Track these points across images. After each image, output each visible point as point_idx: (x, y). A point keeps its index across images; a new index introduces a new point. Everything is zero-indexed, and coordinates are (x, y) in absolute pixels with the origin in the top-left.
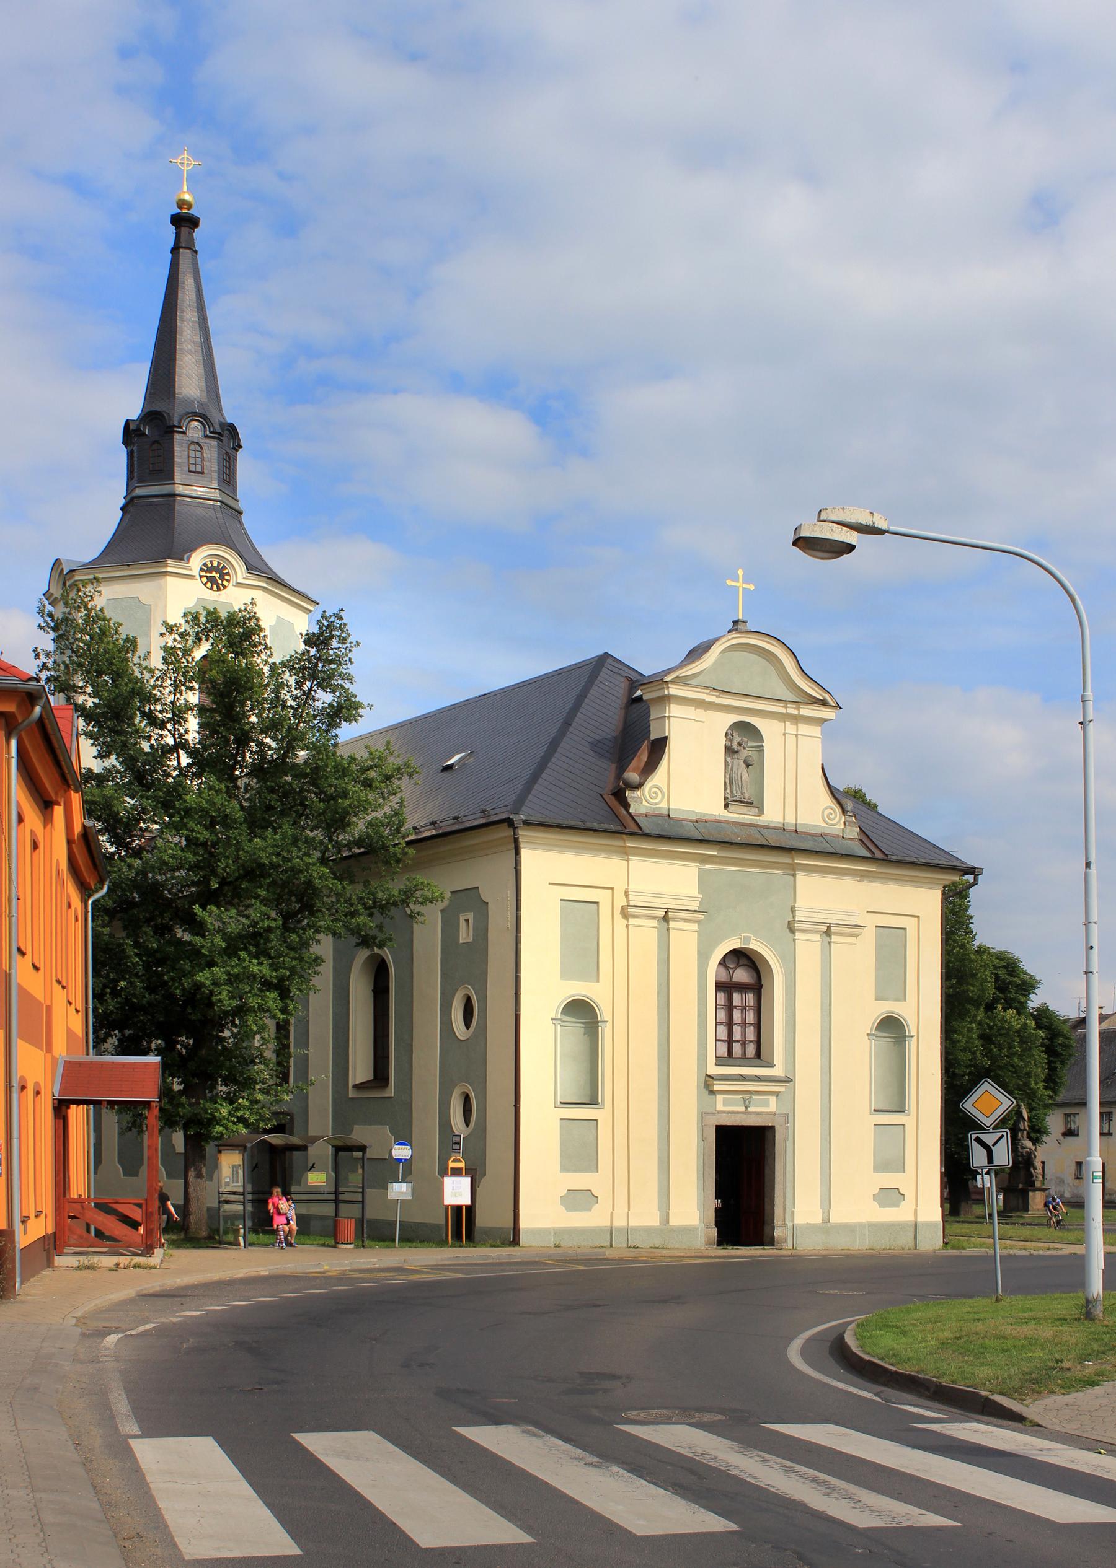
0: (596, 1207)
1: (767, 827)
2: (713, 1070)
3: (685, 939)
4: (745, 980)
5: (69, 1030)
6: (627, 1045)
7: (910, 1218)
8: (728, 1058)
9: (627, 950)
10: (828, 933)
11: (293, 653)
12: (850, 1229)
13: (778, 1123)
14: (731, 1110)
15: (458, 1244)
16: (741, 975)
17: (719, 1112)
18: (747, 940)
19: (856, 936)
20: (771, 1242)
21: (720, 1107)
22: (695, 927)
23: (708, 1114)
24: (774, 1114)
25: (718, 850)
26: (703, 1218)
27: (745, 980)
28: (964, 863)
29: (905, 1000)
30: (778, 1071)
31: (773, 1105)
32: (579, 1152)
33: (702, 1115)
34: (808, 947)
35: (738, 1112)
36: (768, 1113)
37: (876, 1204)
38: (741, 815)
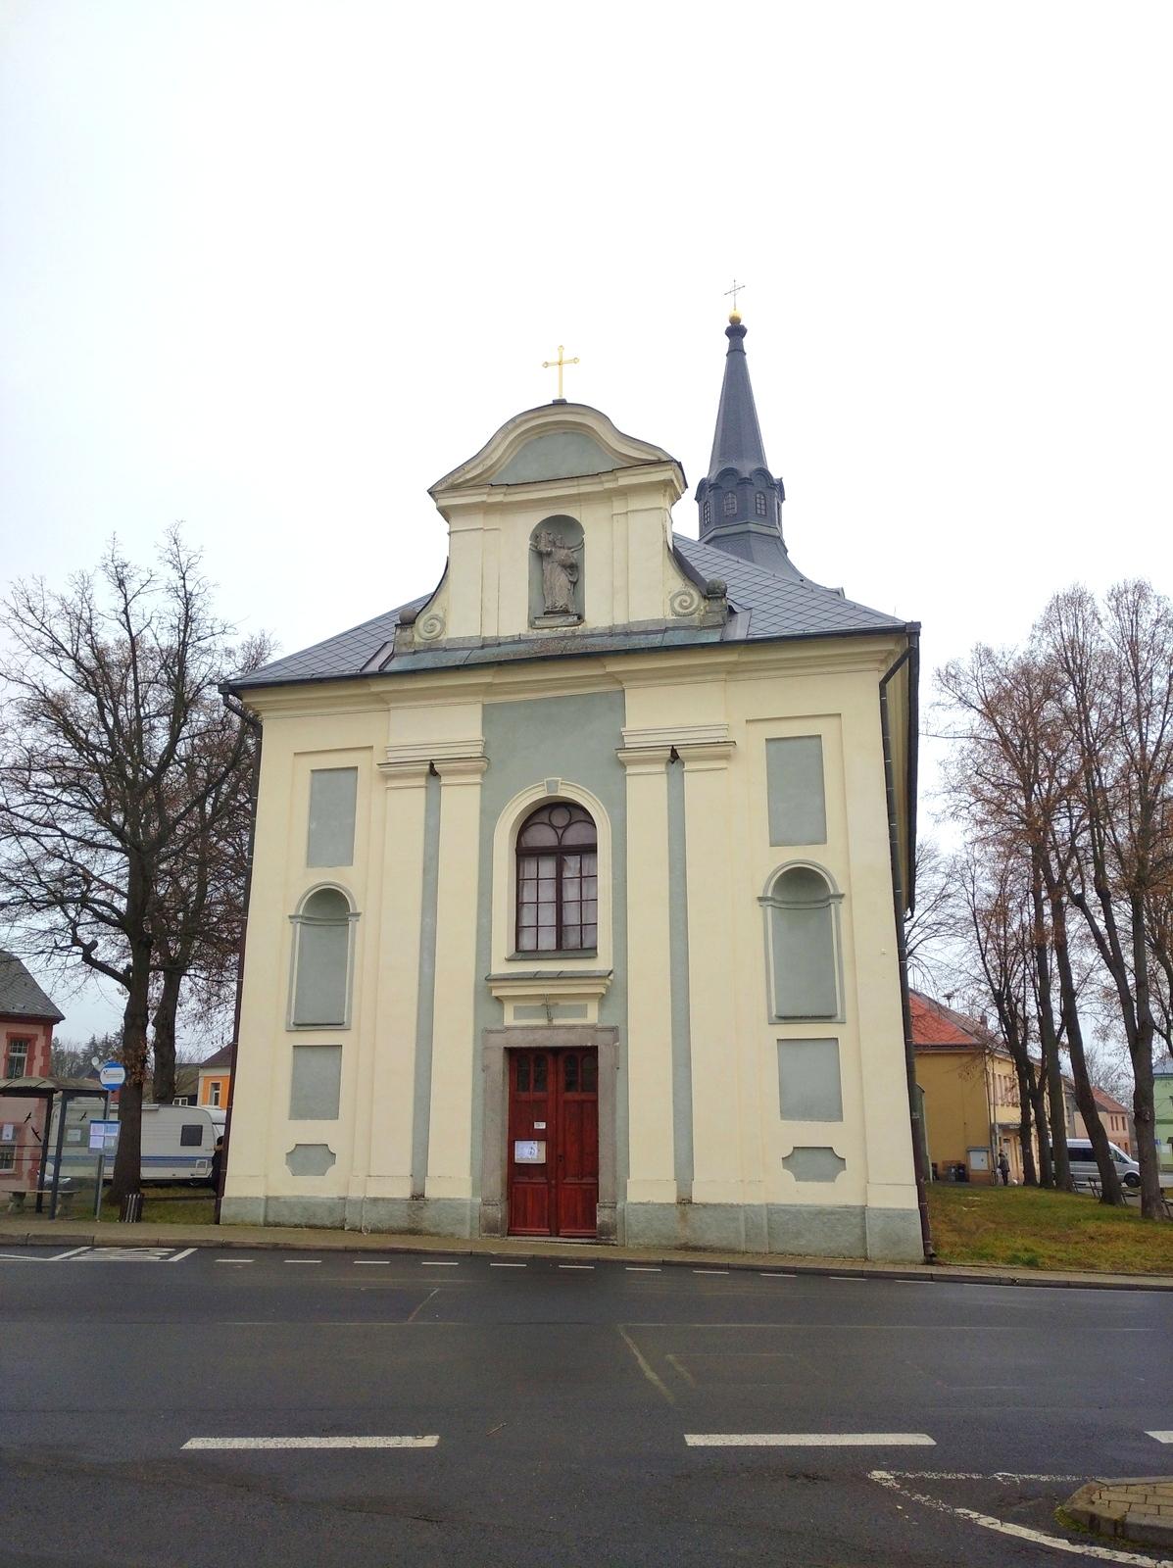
0: (332, 1170)
1: (592, 636)
2: (500, 967)
3: (461, 800)
4: (555, 840)
5: (913, 1011)
6: (382, 941)
7: (854, 1201)
8: (520, 953)
9: (388, 818)
10: (674, 756)
11: (145, 557)
12: (725, 1211)
13: (602, 1041)
14: (522, 1026)
15: (116, 1211)
16: (543, 836)
17: (508, 1029)
18: (550, 785)
19: (726, 757)
20: (599, 1234)
21: (509, 1019)
22: (477, 779)
23: (491, 1032)
24: (592, 1027)
25: (739, 655)
26: (478, 1185)
27: (555, 840)
28: (893, 619)
29: (824, 841)
30: (602, 963)
31: (592, 1015)
32: (315, 1095)
33: (484, 1034)
34: (646, 789)
35: (537, 1028)
36: (584, 1027)
37: (788, 1174)
38: (560, 627)
